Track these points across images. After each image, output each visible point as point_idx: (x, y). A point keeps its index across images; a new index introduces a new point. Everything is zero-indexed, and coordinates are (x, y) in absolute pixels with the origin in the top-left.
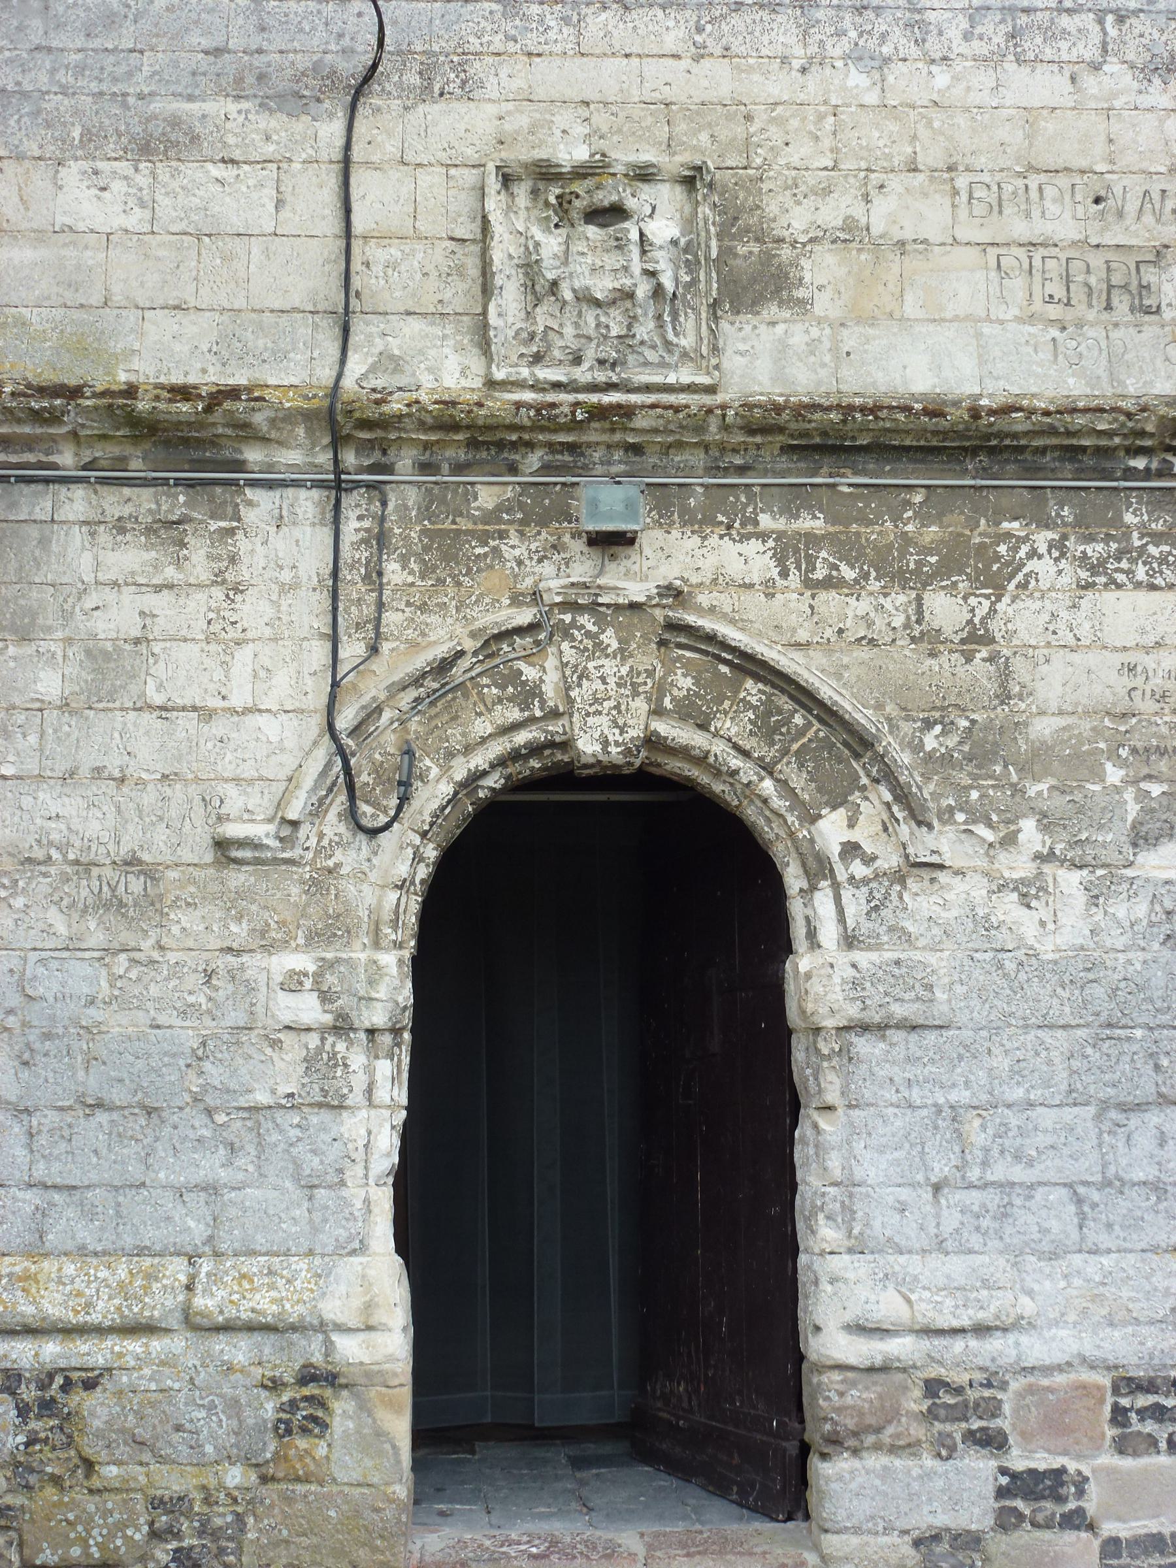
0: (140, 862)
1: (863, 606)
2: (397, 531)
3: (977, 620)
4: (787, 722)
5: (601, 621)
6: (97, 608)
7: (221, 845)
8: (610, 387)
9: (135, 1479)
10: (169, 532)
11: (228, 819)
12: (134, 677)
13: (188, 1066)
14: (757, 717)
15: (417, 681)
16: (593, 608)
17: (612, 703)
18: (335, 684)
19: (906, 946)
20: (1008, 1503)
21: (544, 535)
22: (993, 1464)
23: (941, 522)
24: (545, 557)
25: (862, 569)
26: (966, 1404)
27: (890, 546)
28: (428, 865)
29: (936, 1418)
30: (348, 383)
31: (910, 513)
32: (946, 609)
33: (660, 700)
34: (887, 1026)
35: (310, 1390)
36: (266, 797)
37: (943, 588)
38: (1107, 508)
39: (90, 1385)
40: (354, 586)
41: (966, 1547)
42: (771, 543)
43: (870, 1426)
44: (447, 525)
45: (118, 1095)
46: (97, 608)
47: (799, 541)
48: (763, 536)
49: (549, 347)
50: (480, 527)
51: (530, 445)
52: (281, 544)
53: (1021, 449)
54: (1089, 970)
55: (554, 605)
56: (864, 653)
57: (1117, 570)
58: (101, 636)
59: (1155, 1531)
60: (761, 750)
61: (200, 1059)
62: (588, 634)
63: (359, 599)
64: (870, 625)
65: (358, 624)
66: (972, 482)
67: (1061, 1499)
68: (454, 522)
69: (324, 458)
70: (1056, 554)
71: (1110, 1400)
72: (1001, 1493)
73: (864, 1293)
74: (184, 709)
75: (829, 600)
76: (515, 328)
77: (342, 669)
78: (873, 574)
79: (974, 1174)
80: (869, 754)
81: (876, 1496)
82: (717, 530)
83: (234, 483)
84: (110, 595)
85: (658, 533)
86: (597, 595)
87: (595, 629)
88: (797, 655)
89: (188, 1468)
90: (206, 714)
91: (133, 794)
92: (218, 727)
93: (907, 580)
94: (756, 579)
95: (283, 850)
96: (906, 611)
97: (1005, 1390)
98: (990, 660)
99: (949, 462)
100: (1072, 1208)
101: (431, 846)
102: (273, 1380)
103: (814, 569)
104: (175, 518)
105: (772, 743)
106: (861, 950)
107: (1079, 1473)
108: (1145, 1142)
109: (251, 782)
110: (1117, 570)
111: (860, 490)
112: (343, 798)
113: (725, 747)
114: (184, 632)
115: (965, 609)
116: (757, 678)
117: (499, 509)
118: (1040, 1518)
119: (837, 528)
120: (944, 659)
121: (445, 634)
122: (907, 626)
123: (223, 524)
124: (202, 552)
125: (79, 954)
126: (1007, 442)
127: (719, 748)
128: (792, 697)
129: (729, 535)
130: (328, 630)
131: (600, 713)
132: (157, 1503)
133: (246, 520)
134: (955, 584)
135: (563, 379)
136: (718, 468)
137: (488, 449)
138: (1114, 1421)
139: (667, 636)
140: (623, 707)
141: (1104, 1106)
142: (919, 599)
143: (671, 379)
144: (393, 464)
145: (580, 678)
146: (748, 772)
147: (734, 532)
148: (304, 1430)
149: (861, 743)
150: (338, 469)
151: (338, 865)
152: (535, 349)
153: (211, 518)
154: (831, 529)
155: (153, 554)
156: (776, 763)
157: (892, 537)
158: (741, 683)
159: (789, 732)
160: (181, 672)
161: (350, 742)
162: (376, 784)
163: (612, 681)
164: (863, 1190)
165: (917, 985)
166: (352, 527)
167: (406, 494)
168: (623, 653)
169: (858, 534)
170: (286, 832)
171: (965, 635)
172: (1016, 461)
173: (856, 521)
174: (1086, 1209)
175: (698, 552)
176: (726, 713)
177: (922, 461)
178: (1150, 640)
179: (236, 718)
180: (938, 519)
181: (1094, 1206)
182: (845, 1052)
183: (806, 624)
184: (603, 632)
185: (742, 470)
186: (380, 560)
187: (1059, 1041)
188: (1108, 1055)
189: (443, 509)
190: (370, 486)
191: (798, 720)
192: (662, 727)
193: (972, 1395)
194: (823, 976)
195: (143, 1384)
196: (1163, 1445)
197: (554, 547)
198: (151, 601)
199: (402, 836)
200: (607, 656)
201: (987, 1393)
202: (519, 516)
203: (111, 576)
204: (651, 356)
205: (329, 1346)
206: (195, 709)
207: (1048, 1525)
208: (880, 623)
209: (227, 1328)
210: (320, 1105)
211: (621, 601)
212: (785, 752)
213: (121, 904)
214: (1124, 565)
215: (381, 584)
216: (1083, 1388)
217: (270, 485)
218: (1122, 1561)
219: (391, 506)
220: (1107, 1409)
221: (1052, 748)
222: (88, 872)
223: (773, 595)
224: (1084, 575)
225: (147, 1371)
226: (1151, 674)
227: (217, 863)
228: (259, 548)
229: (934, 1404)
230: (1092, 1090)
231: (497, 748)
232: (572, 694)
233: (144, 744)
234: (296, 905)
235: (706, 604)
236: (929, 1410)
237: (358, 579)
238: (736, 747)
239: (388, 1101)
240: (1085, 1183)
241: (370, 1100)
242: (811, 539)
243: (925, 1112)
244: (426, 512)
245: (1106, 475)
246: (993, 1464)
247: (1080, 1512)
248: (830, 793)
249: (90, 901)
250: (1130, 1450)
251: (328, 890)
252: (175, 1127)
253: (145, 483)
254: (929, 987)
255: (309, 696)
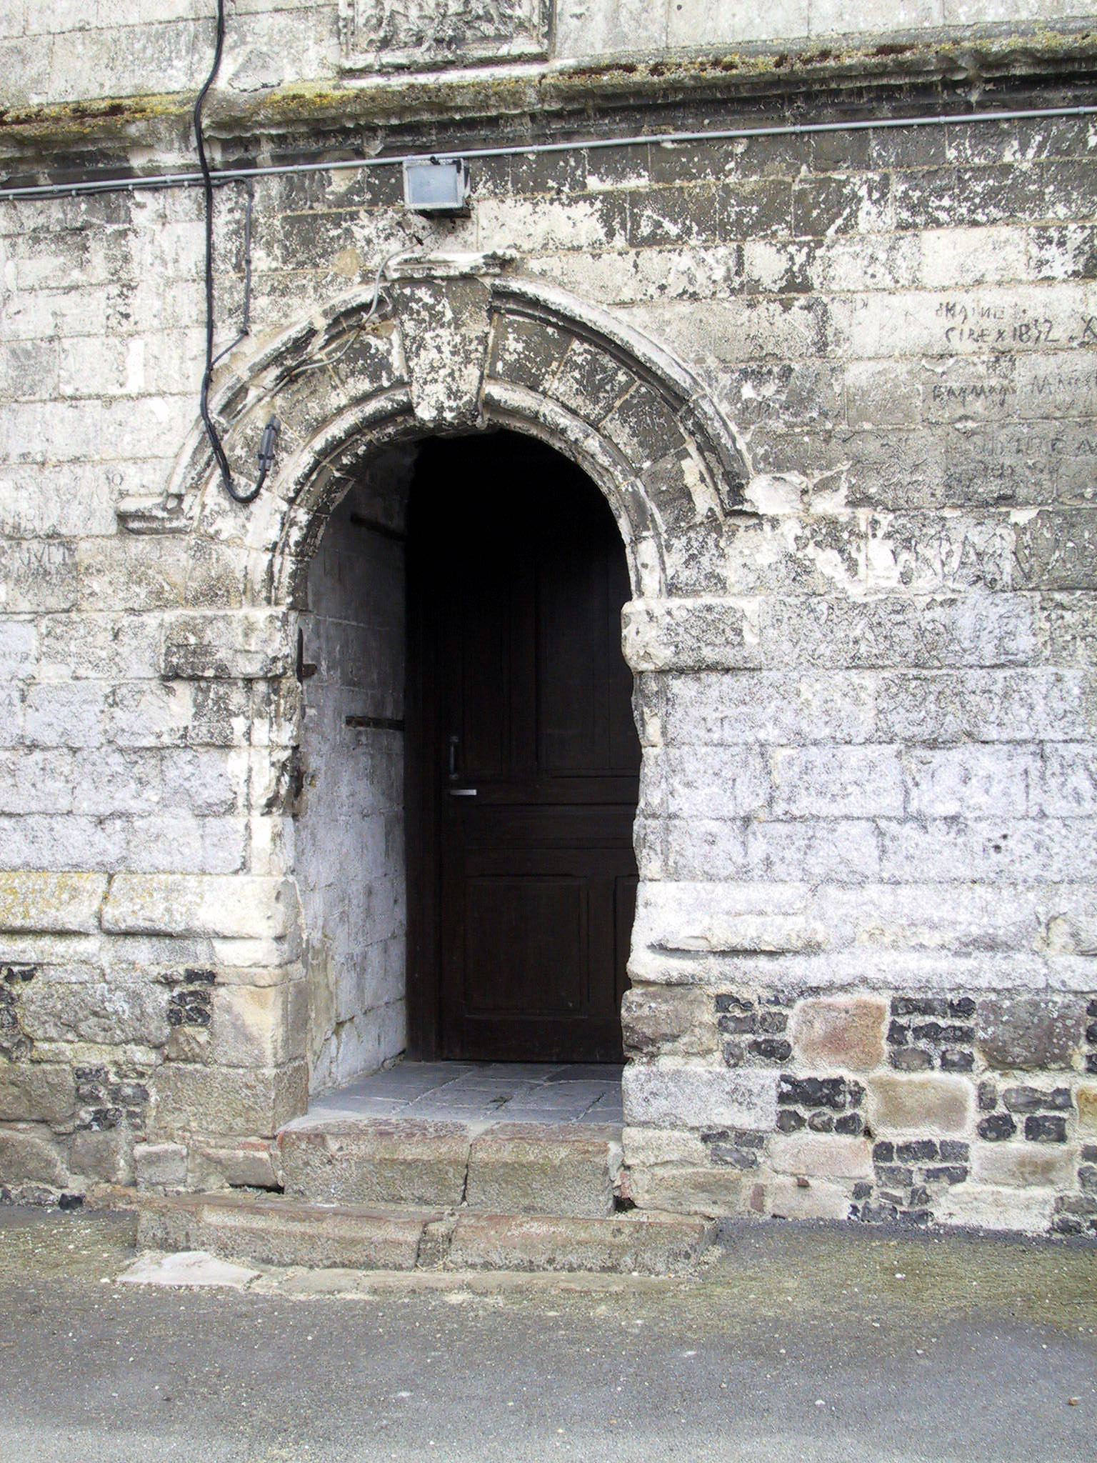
0: (59, 535)
1: (683, 261)
2: (262, 220)
3: (795, 268)
4: (612, 379)
5: (437, 294)
6: (19, 312)
7: (122, 517)
8: (447, 65)
9: (63, 1053)
10: (74, 237)
11: (128, 495)
12: (49, 371)
13: (102, 712)
14: (583, 376)
15: (277, 358)
16: (429, 281)
17: (447, 371)
18: (210, 367)
19: (721, 592)
20: (791, 1108)
21: (390, 213)
22: (776, 1073)
23: (762, 171)
24: (392, 234)
25: (684, 224)
26: (753, 1018)
27: (711, 200)
28: (301, 528)
29: (726, 1029)
30: (221, 84)
31: (732, 165)
32: (766, 261)
33: (493, 365)
34: (700, 670)
35: (195, 986)
36: (158, 473)
37: (763, 237)
38: (930, 144)
39: (27, 977)
40: (226, 275)
41: (750, 1143)
42: (598, 205)
43: (666, 1035)
44: (306, 212)
45: (50, 738)
46: (19, 312)
47: (624, 201)
48: (590, 198)
49: (395, 33)
50: (334, 210)
51: (373, 129)
52: (165, 239)
53: (837, 93)
54: (898, 612)
55: (394, 281)
56: (685, 308)
57: (937, 208)
58: (24, 337)
59: (926, 1139)
60: (588, 409)
61: (111, 706)
62: (425, 306)
63: (231, 287)
64: (691, 281)
65: (230, 310)
66: (792, 129)
67: (837, 1107)
68: (311, 208)
69: (193, 158)
70: (876, 195)
71: (888, 1018)
72: (783, 1098)
73: (671, 919)
74: (90, 397)
75: (650, 255)
76: (366, 15)
77: (216, 354)
78: (695, 228)
79: (779, 809)
80: (685, 408)
81: (678, 1096)
82: (548, 197)
83: (122, 189)
84: (28, 299)
85: (493, 203)
86: (430, 269)
87: (431, 301)
88: (621, 314)
89: (104, 1047)
90: (109, 401)
91: (52, 476)
92: (120, 411)
93: (728, 233)
94: (583, 241)
95: (170, 520)
96: (726, 263)
97: (791, 1007)
98: (808, 308)
99: (767, 110)
100: (873, 841)
101: (302, 511)
102: (165, 977)
103: (639, 227)
104: (78, 225)
105: (596, 402)
106: (680, 597)
107: (856, 1084)
108: (949, 777)
109: (144, 460)
110: (937, 208)
111: (683, 145)
112: (219, 471)
113: (552, 404)
114: (87, 329)
115: (785, 257)
116: (583, 340)
117: (351, 191)
118: (817, 1121)
119: (661, 185)
120: (761, 309)
121: (307, 313)
122: (727, 278)
123: (116, 227)
124: (101, 254)
125: (16, 617)
126: (817, 87)
127: (549, 410)
128: (614, 356)
129: (559, 199)
130: (204, 317)
131: (436, 381)
132: (80, 1074)
133: (135, 221)
134: (774, 234)
135: (404, 61)
136: (545, 135)
137: (335, 137)
138: (890, 1038)
139: (497, 303)
140: (457, 374)
141: (910, 742)
142: (740, 250)
143: (504, 50)
144: (254, 158)
145: (418, 348)
146: (574, 429)
147: (563, 197)
148: (190, 1019)
149: (673, 398)
150: (205, 167)
151: (218, 532)
152: (382, 34)
153: (107, 222)
154: (656, 186)
155: (62, 259)
156: (600, 420)
157: (714, 190)
158: (569, 344)
159: (612, 390)
160: (84, 364)
161: (222, 420)
162: (249, 457)
163: (446, 349)
164: (677, 822)
165: (728, 630)
166: (223, 221)
167: (270, 188)
168: (457, 323)
169: (681, 189)
170: (172, 504)
171: (784, 283)
172: (833, 104)
173: (679, 176)
174: (887, 842)
175: (530, 219)
176: (554, 373)
177: (741, 113)
178: (968, 279)
179: (131, 403)
180: (760, 168)
181: (894, 839)
182: (662, 692)
183: (630, 282)
184: (439, 303)
185: (568, 136)
186: (248, 249)
187: (870, 681)
188: (914, 696)
189: (302, 195)
190: (238, 181)
191: (621, 377)
192: (496, 391)
193: (759, 1011)
194: (648, 627)
195: (66, 978)
196: (937, 1062)
197: (399, 224)
198: (66, 303)
199: (270, 506)
200: (442, 326)
201: (774, 1009)
202: (368, 196)
203: (28, 283)
204: (488, 29)
205: (212, 953)
206: (98, 397)
207: (825, 1128)
208: (701, 276)
209: (129, 934)
210: (208, 744)
211: (452, 273)
212: (609, 409)
213: (47, 573)
214: (946, 202)
215: (250, 272)
216: (865, 1010)
217: (155, 188)
218: (893, 1164)
219: (257, 196)
220: (885, 1029)
221: (868, 392)
222: (19, 544)
223: (600, 256)
224: (905, 215)
225: (69, 967)
226: (970, 313)
227: (120, 532)
228: (148, 247)
229: (725, 1017)
230: (897, 728)
231: (351, 418)
232: (412, 364)
233: (54, 429)
234: (184, 569)
235: (537, 269)
236: (720, 1023)
237: (230, 268)
238: (564, 406)
239: (266, 742)
240: (889, 819)
241: (249, 739)
242: (636, 198)
243: (735, 750)
244: (287, 202)
245: (929, 111)
246: (776, 1073)
247: (854, 1118)
248: (651, 447)
249: (22, 571)
250: (904, 1065)
251: (210, 554)
252: (94, 764)
253: (51, 196)
254: (739, 632)
255: (191, 379)
